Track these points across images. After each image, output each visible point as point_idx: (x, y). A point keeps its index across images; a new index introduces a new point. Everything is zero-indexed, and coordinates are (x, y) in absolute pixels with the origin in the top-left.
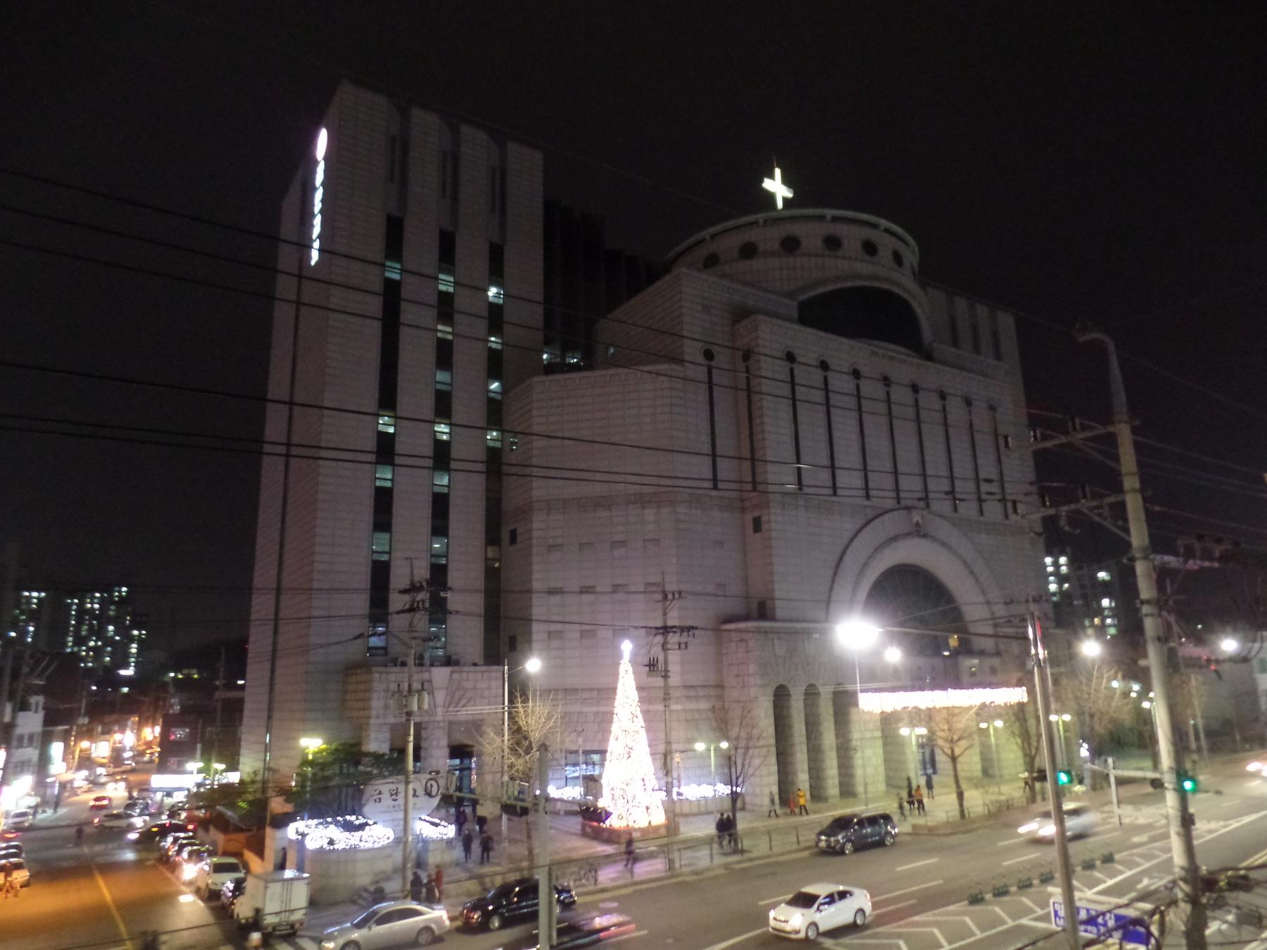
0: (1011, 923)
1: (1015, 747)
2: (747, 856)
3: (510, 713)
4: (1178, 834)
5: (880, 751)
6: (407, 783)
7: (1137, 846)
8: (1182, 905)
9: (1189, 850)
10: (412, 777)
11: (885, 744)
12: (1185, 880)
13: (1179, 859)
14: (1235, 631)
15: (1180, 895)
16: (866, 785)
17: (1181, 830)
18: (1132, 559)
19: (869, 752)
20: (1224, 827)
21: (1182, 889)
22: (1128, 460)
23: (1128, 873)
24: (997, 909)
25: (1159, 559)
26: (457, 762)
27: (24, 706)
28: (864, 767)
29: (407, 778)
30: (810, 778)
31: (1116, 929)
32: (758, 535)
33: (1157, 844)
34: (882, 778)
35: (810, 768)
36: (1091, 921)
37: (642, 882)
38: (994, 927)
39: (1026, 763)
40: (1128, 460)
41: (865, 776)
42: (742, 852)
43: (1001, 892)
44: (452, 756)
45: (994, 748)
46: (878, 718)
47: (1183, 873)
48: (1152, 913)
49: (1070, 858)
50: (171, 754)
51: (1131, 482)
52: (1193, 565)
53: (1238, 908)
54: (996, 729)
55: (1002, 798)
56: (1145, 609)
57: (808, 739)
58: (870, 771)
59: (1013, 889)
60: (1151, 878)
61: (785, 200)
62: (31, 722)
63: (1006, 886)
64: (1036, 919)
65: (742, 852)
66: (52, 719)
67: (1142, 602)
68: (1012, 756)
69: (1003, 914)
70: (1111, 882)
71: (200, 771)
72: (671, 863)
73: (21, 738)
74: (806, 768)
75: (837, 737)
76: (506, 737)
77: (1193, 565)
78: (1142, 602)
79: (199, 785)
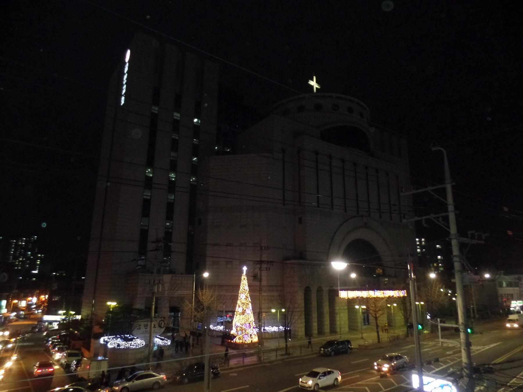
0: (397, 385)
1: (401, 315)
2: (291, 356)
4: (464, 349)
6: (151, 322)
8: (465, 378)
12: (466, 368)
13: (464, 360)
16: (340, 328)
17: (466, 348)
19: (342, 315)
23: (445, 366)
26: (173, 314)
30: (318, 325)
34: (347, 326)
37: (247, 366)
42: (289, 354)
44: (171, 312)
47: (466, 365)
51: (451, 208)
55: (395, 335)
60: (453, 368)
68: (399, 318)
71: (64, 314)
74: (316, 320)
76: (193, 304)
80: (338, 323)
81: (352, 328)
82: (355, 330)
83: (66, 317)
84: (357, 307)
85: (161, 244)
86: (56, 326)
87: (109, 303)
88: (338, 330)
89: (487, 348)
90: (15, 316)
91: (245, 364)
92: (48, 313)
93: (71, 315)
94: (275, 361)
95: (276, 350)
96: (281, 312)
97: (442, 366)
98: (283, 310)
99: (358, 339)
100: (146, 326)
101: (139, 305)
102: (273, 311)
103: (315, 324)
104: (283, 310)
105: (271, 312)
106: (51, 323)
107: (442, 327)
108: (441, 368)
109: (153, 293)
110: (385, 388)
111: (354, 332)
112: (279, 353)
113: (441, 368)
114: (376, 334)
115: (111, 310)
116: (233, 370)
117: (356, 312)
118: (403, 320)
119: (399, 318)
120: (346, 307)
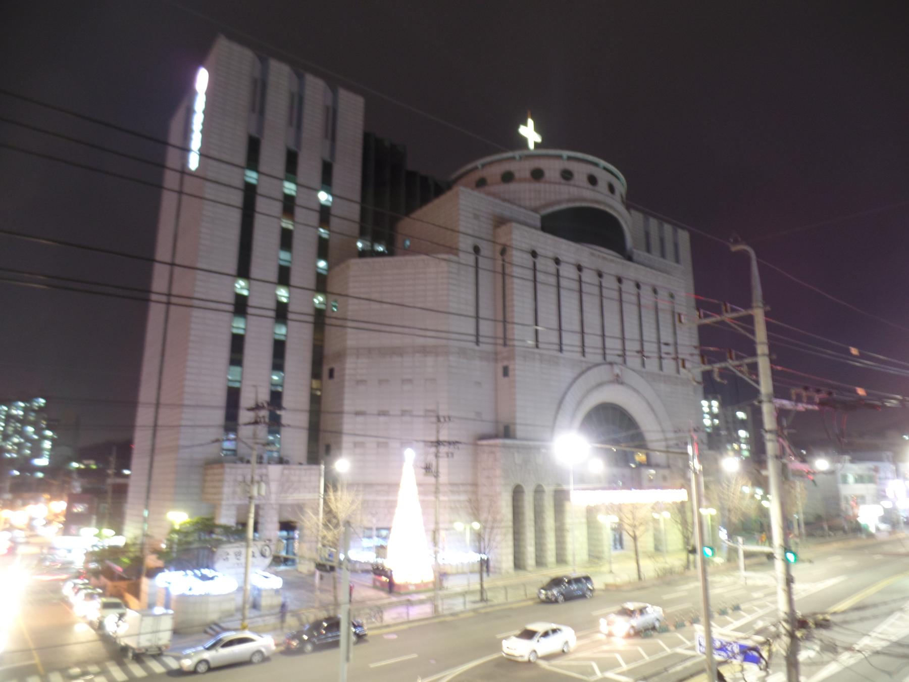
0: (669, 651)
18: (760, 402)
22: (761, 334)
32: (507, 379)
40: (761, 334)
42: (486, 601)
51: (762, 349)
94: (462, 612)
100: (238, 555)
103: (530, 550)
112: (469, 598)
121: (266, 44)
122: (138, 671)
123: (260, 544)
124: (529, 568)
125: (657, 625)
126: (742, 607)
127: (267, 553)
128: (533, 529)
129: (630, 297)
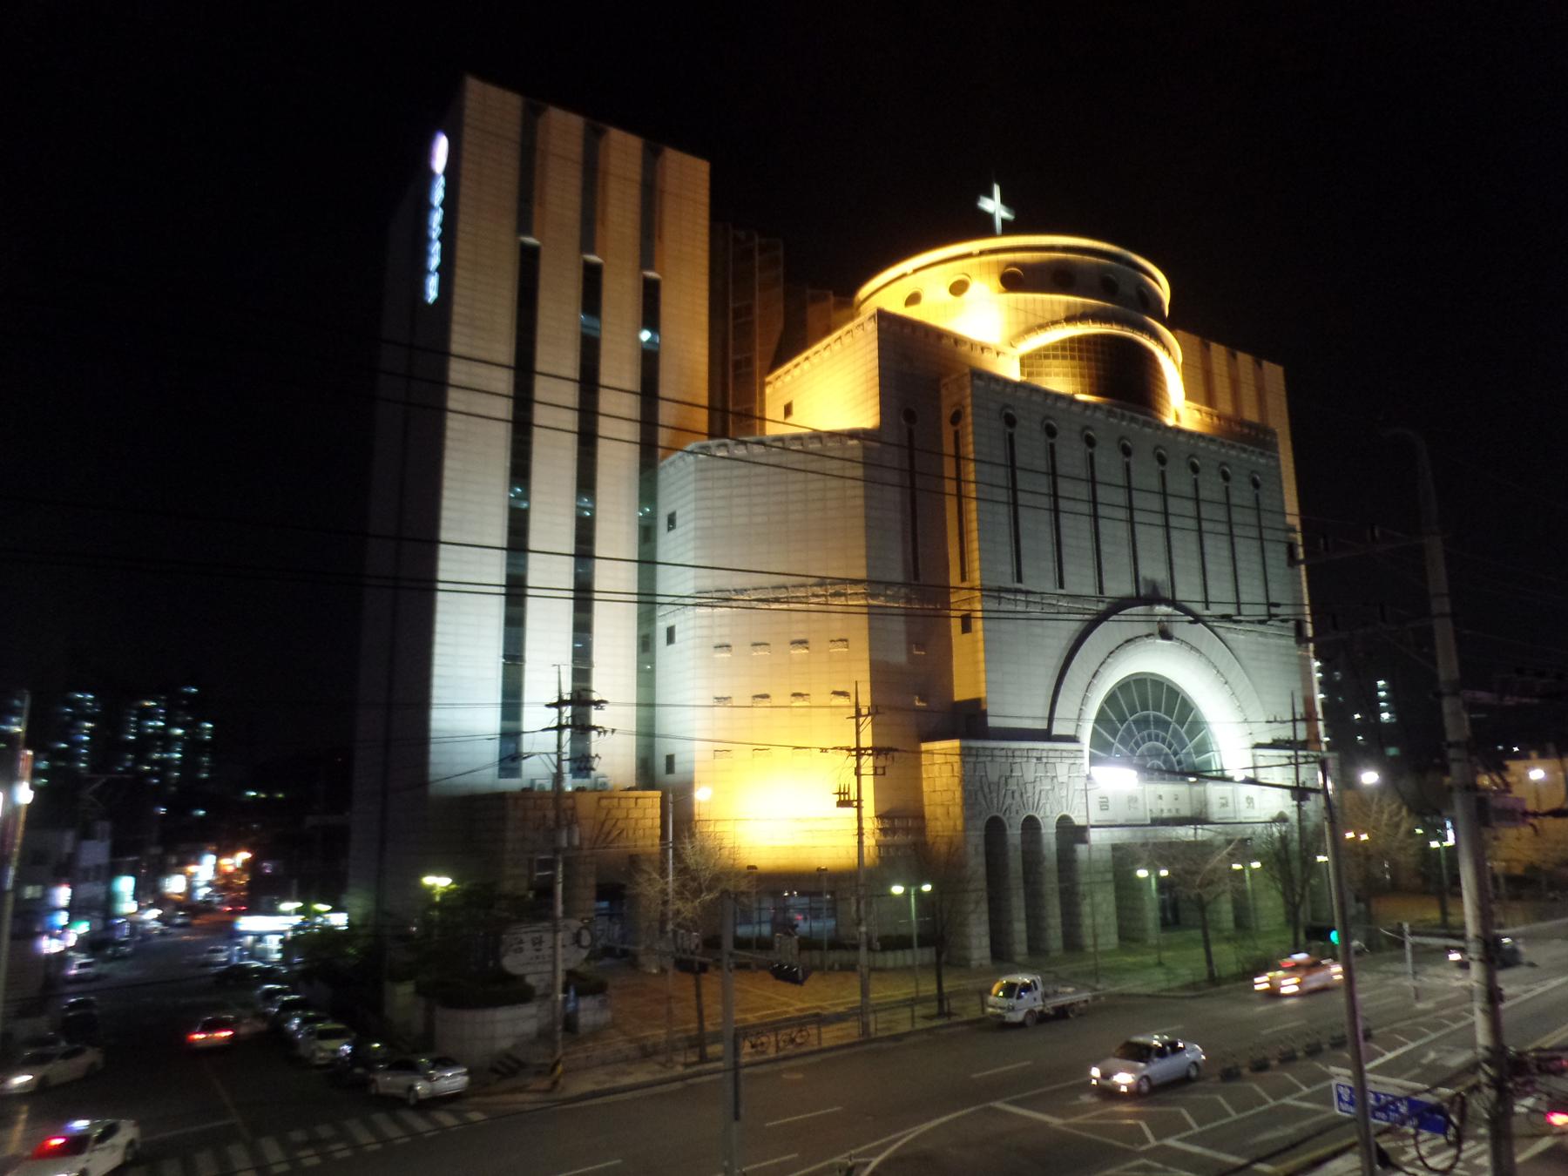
0: (1272, 1103)
1: (1274, 893)
2: (954, 1019)
3: (675, 850)
4: (1483, 1011)
5: (1112, 898)
6: (556, 932)
7: (1425, 1013)
8: (1486, 1090)
9: (1496, 1028)
10: (561, 924)
11: (1118, 888)
12: (1487, 1061)
13: (1482, 1037)
14: (1543, 755)
15: (1483, 1078)
16: (1095, 937)
17: (1487, 1007)
18: (1439, 695)
19: (1099, 898)
20: (1526, 992)
21: (1486, 1073)
22: (1438, 577)
23: (1412, 1045)
24: (1258, 1089)
25: (1468, 694)
26: (605, 904)
27: (86, 834)
28: (1093, 915)
29: (555, 925)
30: (1028, 927)
31: (1410, 1118)
32: (967, 635)
33: (1444, 1012)
34: (1113, 929)
35: (1027, 916)
36: (1384, 1108)
37: (831, 1049)
38: (564, 902)
39: (1287, 913)
40: (1438, 577)
41: (1094, 927)
42: (949, 1014)
43: (1260, 1066)
44: (600, 898)
45: (1250, 895)
46: (1108, 855)
47: (1486, 1054)
48: (1451, 1100)
49: (1351, 1038)
50: (258, 893)
51: (1441, 605)
52: (1510, 701)
53: (1549, 1095)
54: (1253, 871)
55: (1259, 953)
56: (1452, 753)
57: (1026, 882)
58: (1100, 920)
59: (1274, 1063)
60: (1438, 1051)
61: (1004, 221)
62: (95, 852)
63: (1265, 1059)
64: (1302, 1099)
65: (949, 1014)
66: (118, 850)
67: (1450, 745)
68: (1270, 904)
69: (1263, 1094)
70: (1390, 1056)
71: (298, 912)
72: (865, 1026)
73: (86, 871)
74: (1023, 915)
75: (1061, 880)
76: (671, 878)
77: (1510, 701)
78: (1450, 745)
79: (296, 928)
80: (1087, 921)
81: (1129, 935)
82: (1135, 940)
83: (304, 921)
84: (1142, 873)
85: (568, 711)
86: (273, 943)
87: (428, 880)
88: (1088, 941)
89: (1540, 990)
90: (159, 919)
91: (825, 1045)
92: (252, 911)
93: (319, 914)
94: (909, 1034)
95: (912, 1002)
96: (919, 894)
97: (1402, 1044)
98: (927, 888)
99: (1145, 967)
100: (537, 943)
101: (515, 880)
102: (897, 890)
103: (1019, 927)
104: (927, 888)
105: (891, 895)
106: (260, 937)
107: (1414, 946)
108: (1400, 1051)
109: (556, 851)
110: (1238, 1112)
111: (1134, 945)
112: (920, 1010)
113: (1400, 1051)
114: (1202, 950)
115: (438, 899)
116: (792, 1063)
117: (1140, 889)
118: (1282, 911)
119: (1270, 904)
120: (1110, 876)
121: (539, 91)
122: (420, 1124)
123: (575, 924)
124: (1019, 959)
125: (1193, 1073)
126: (1375, 1032)
127: (586, 939)
128: (1021, 892)
129: (1180, 481)
